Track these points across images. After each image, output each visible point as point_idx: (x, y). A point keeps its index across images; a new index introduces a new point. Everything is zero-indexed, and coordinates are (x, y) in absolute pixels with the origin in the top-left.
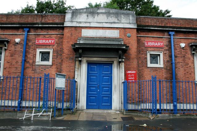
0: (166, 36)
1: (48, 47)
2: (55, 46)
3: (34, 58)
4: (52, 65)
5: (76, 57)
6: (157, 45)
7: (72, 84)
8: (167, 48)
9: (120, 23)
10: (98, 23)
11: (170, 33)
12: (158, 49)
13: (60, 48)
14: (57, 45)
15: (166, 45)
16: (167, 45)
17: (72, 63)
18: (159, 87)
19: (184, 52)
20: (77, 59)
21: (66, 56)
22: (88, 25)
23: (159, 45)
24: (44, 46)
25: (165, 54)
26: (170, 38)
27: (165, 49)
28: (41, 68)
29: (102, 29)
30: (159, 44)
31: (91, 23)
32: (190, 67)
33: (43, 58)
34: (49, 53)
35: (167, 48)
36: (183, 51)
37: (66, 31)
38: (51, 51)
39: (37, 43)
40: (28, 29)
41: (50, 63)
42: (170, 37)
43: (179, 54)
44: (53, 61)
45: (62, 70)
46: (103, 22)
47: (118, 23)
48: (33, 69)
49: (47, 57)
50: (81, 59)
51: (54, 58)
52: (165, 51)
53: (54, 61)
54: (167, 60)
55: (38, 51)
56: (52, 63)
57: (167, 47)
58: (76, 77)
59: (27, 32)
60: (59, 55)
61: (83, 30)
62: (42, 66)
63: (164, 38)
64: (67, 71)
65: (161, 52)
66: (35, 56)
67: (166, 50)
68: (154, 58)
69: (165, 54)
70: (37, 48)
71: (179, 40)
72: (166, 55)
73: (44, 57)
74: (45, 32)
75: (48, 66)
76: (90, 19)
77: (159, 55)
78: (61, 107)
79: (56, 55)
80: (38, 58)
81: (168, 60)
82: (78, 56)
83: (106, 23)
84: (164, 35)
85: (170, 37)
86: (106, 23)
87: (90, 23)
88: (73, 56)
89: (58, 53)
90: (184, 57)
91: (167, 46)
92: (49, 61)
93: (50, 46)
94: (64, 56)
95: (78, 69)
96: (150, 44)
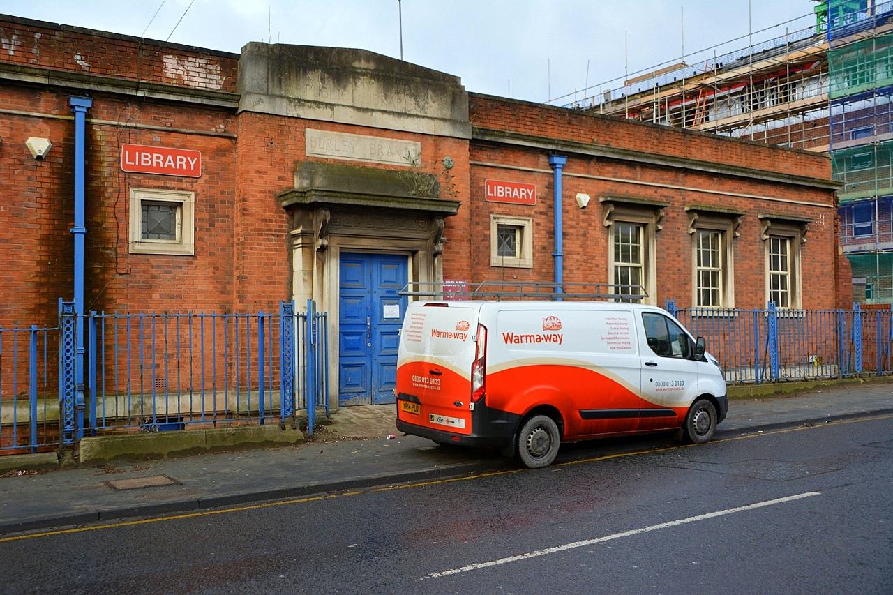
1: (172, 184)
4: (195, 257)
9: (424, 117)
10: (358, 109)
13: (222, 192)
14: (207, 177)
15: (540, 198)
16: (544, 198)
17: (276, 250)
19: (583, 221)
22: (323, 114)
24: (157, 177)
25: (538, 224)
32: (597, 266)
34: (146, 205)
36: (582, 217)
38: (189, 201)
39: (127, 162)
42: (551, 172)
43: (572, 227)
44: (197, 239)
46: (373, 110)
51: (201, 229)
52: (538, 215)
54: (540, 243)
55: (137, 196)
57: (543, 202)
60: (218, 216)
61: (310, 133)
63: (536, 174)
65: (529, 220)
67: (542, 213)
68: (160, 218)
71: (575, 182)
74: (155, 118)
76: (330, 95)
79: (206, 215)
81: (546, 244)
84: (536, 165)
85: (551, 172)
88: (282, 226)
89: (212, 214)
90: (584, 235)
91: (543, 200)
93: (180, 179)
95: (428, 274)
96: (501, 192)
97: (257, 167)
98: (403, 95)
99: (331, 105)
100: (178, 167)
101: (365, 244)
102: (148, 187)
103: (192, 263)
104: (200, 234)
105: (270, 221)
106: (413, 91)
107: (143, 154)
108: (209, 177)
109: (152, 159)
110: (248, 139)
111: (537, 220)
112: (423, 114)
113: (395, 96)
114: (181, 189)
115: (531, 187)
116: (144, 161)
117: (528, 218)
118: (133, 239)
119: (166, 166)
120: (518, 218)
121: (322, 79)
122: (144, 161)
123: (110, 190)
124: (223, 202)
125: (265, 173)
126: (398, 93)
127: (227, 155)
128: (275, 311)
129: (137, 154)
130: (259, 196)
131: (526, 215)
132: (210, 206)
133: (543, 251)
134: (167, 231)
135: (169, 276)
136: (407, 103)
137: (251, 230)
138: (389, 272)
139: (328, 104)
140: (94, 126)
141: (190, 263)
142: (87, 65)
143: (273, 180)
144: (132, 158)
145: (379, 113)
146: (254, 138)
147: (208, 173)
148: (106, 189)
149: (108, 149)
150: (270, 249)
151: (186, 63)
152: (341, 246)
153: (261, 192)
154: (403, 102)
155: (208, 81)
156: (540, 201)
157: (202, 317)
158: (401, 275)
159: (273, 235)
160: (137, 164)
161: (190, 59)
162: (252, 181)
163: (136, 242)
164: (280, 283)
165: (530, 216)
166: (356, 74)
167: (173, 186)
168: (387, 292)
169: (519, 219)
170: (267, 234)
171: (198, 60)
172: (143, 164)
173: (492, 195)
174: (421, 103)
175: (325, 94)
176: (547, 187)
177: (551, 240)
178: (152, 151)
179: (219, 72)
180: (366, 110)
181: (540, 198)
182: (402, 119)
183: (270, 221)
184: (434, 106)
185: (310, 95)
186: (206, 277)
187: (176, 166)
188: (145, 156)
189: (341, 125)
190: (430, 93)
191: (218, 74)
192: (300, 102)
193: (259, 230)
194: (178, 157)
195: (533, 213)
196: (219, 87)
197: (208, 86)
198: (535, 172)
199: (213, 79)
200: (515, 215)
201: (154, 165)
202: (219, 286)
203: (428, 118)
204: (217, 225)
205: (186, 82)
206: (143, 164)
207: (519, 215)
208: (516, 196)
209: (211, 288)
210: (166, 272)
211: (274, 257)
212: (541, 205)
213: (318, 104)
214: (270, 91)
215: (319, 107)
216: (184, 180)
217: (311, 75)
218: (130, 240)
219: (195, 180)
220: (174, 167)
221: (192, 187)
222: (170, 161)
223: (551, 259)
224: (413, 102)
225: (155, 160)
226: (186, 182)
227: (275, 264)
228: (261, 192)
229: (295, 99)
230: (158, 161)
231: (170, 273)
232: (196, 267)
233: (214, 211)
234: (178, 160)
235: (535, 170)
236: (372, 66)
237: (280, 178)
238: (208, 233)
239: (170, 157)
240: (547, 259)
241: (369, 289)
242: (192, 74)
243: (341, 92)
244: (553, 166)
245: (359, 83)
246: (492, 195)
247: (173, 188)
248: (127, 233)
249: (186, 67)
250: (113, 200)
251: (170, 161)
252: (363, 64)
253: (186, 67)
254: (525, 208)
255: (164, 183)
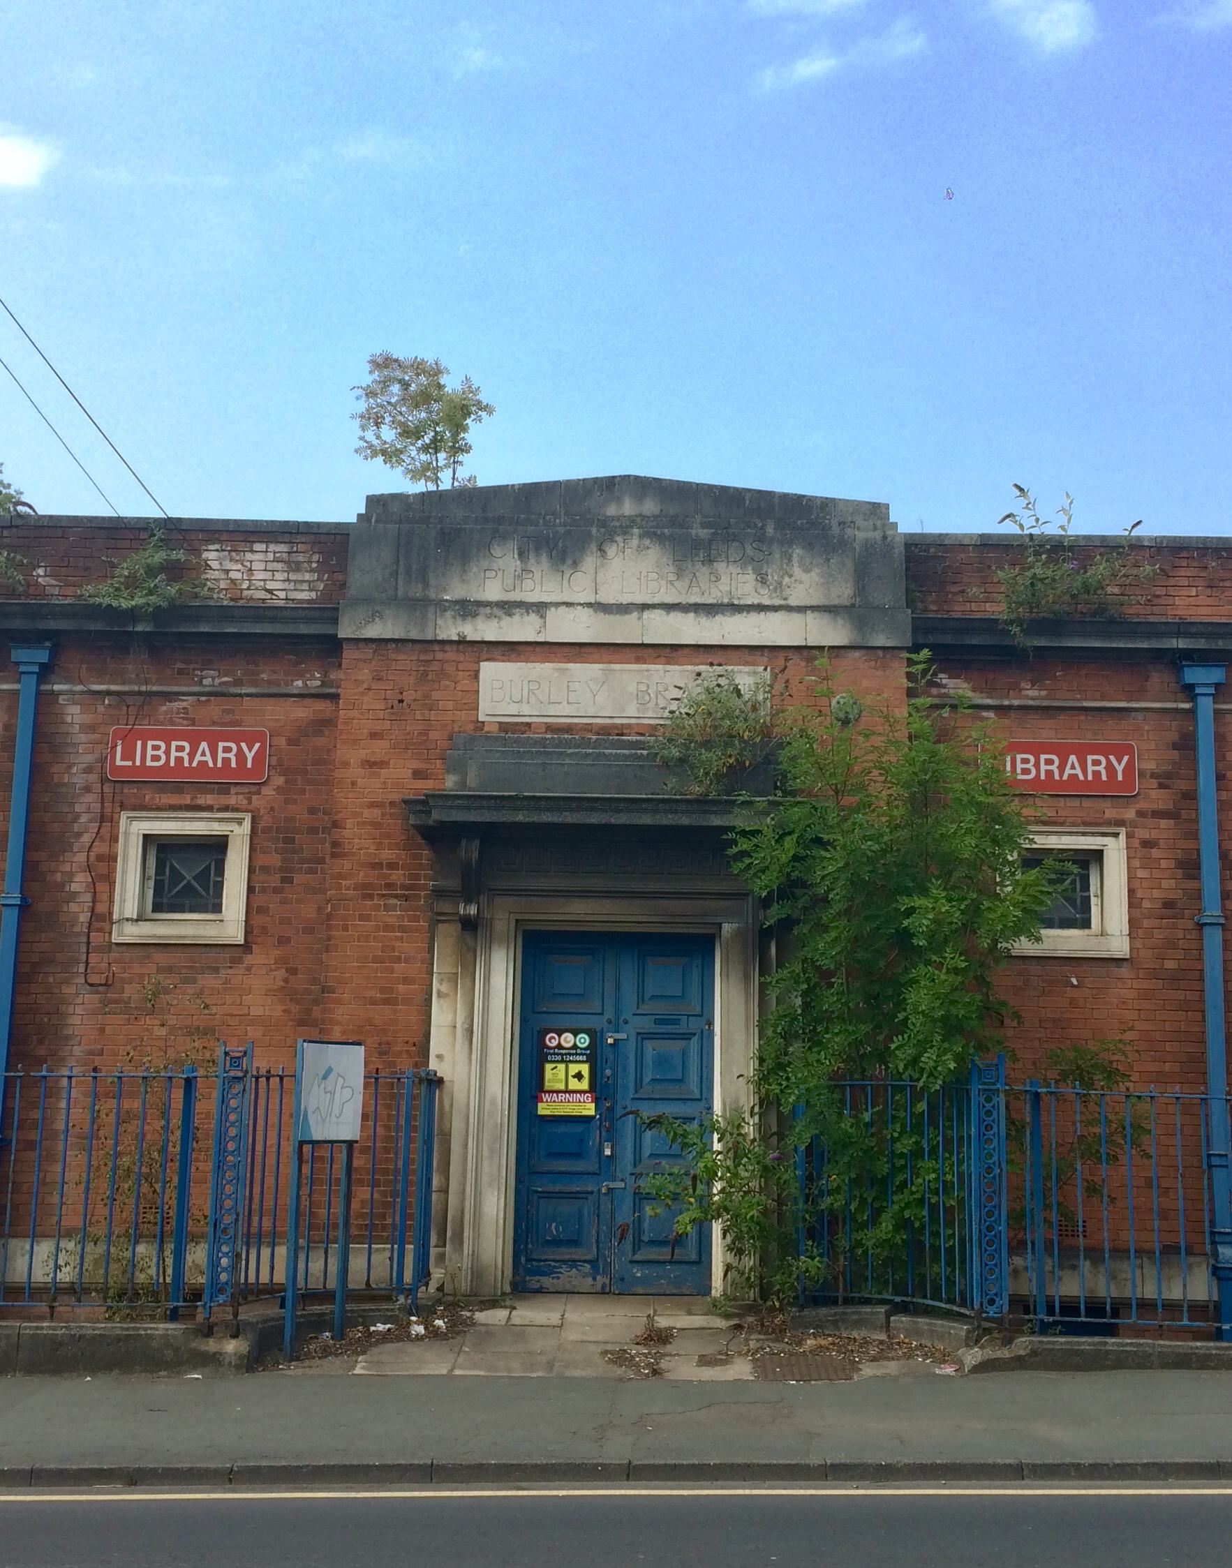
0: (1156, 698)
1: (209, 799)
2: (266, 791)
3: (102, 887)
4: (247, 947)
5: (439, 893)
6: (1078, 771)
7: (407, 1093)
8: (1159, 798)
9: (775, 609)
11: (1194, 675)
12: (1087, 803)
13: (312, 811)
14: (279, 781)
15: (1153, 775)
16: (1169, 775)
17: (402, 929)
18: (523, 900)
20: (446, 907)
21: (361, 877)
23: (1097, 774)
24: (178, 788)
25: (1147, 844)
26: (1192, 712)
27: (1143, 805)
28: (160, 970)
29: (638, 660)
30: (1096, 766)
31: (551, 613)
33: (174, 883)
34: (218, 846)
35: (1159, 798)
37: (355, 675)
38: (239, 834)
39: (119, 762)
40: (43, 656)
41: (230, 921)
42: (1187, 706)
45: (331, 990)
46: (645, 607)
47: (761, 608)
48: (94, 979)
49: (203, 877)
50: (473, 910)
51: (263, 890)
52: (1150, 821)
53: (262, 910)
54: (1156, 894)
56: (248, 932)
57: (1161, 786)
58: (437, 1044)
59: (34, 678)
60: (302, 861)
61: (490, 671)
62: (162, 958)
63: (1140, 716)
64: (373, 993)
65: (1116, 835)
66: (103, 872)
67: (1157, 814)
68: (184, 874)
69: (1141, 850)
70: (123, 807)
72: (1155, 853)
73: (176, 876)
74: (180, 672)
75: (213, 954)
76: (541, 585)
77: (1098, 855)
78: (332, 1284)
79: (275, 860)
80: (131, 885)
81: (1171, 895)
82: (454, 883)
83: (669, 607)
84: (1140, 694)
85: (1187, 706)
86: (669, 607)
87: (543, 617)
88: (417, 877)
89: (292, 852)
91: (1164, 780)
92: (217, 908)
93: (224, 789)
94: (340, 876)
97: (363, 754)
98: (724, 564)
99: (540, 608)
100: (219, 764)
101: (582, 912)
102: (159, 809)
103: (240, 961)
104: (260, 900)
105: (392, 866)
106: (749, 551)
107: (150, 743)
108: (286, 782)
109: (1037, 765)
110: (361, 689)
111: (1142, 833)
112: (777, 602)
113: (704, 570)
114: (226, 809)
115: (1119, 752)
116: (152, 756)
117: (1115, 830)
118: (121, 912)
119: (1065, 777)
120: (1081, 829)
121: (521, 554)
122: (152, 756)
123: (83, 819)
124: (313, 830)
125: (382, 764)
126: (711, 561)
127: (326, 733)
128: (393, 1064)
129: (139, 743)
130: (368, 814)
131: (1109, 823)
132: (285, 841)
133: (1169, 912)
134: (206, 897)
135: (191, 989)
136: (735, 581)
137: (348, 889)
138: (664, 977)
139: (534, 604)
140: (61, 697)
141: (236, 961)
142: (54, 582)
143: (401, 779)
144: (129, 754)
145: (658, 612)
146: (362, 694)
147: (285, 772)
148: (77, 817)
149: (83, 738)
150: (388, 928)
151: (249, 556)
152: (519, 917)
153: (372, 805)
154: (725, 579)
155: (292, 586)
156: (1155, 783)
157: (281, 1078)
158: (695, 991)
159: (396, 896)
160: (138, 763)
161: (257, 547)
162: (353, 784)
163: (127, 920)
164: (407, 1001)
165: (1120, 823)
166: (611, 531)
167: (209, 802)
168: (656, 1022)
169: (1084, 834)
170: (384, 895)
171: (272, 547)
172: (149, 763)
173: (130, 763)
174: (773, 577)
175: (528, 584)
176: (1175, 746)
177: (1192, 884)
178: (168, 737)
179: (314, 565)
180: (623, 609)
181: (1153, 775)
182: (719, 618)
183: (392, 866)
184: (805, 584)
185: (493, 591)
186: (269, 990)
187: (215, 761)
188: (156, 748)
189: (603, 650)
190: (798, 552)
191: (312, 571)
192: (468, 609)
193: (365, 886)
194: (1090, 758)
195: (1130, 814)
196: (313, 595)
197: (292, 595)
198: (1136, 710)
199: (302, 582)
200: (1074, 824)
201: (1043, 777)
202: (295, 1008)
203: (789, 609)
204: (298, 878)
205: (246, 593)
206: (149, 763)
207: (1086, 824)
208: (203, 764)
209: (278, 1012)
210: (186, 981)
211: (398, 944)
212: (1154, 794)
213: (508, 608)
214: (400, 592)
215: (510, 615)
216: (233, 790)
217: (497, 551)
218: (115, 917)
219: (255, 789)
220: (211, 765)
221: (250, 803)
222: (1073, 767)
223: (1194, 935)
224: (750, 577)
225: (1043, 767)
226: (237, 794)
227: (398, 960)
228: (372, 805)
229: (456, 602)
230: (1096, 768)
231: (194, 981)
232: (249, 969)
233: (294, 852)
234: (220, 749)
235: (1135, 705)
236: (650, 507)
237: (418, 774)
238: (278, 897)
239: (1073, 758)
240: (1180, 934)
241: (609, 1014)
242: (259, 575)
243: (566, 576)
244: (1189, 691)
245: (611, 551)
246: (130, 763)
247: (209, 808)
248: (111, 901)
249: (248, 564)
250: (86, 838)
251: (1073, 767)
252: (628, 508)
253: (248, 564)
254: (1105, 804)
255: (192, 799)
